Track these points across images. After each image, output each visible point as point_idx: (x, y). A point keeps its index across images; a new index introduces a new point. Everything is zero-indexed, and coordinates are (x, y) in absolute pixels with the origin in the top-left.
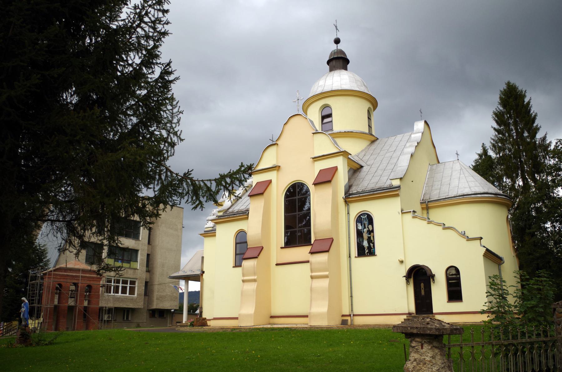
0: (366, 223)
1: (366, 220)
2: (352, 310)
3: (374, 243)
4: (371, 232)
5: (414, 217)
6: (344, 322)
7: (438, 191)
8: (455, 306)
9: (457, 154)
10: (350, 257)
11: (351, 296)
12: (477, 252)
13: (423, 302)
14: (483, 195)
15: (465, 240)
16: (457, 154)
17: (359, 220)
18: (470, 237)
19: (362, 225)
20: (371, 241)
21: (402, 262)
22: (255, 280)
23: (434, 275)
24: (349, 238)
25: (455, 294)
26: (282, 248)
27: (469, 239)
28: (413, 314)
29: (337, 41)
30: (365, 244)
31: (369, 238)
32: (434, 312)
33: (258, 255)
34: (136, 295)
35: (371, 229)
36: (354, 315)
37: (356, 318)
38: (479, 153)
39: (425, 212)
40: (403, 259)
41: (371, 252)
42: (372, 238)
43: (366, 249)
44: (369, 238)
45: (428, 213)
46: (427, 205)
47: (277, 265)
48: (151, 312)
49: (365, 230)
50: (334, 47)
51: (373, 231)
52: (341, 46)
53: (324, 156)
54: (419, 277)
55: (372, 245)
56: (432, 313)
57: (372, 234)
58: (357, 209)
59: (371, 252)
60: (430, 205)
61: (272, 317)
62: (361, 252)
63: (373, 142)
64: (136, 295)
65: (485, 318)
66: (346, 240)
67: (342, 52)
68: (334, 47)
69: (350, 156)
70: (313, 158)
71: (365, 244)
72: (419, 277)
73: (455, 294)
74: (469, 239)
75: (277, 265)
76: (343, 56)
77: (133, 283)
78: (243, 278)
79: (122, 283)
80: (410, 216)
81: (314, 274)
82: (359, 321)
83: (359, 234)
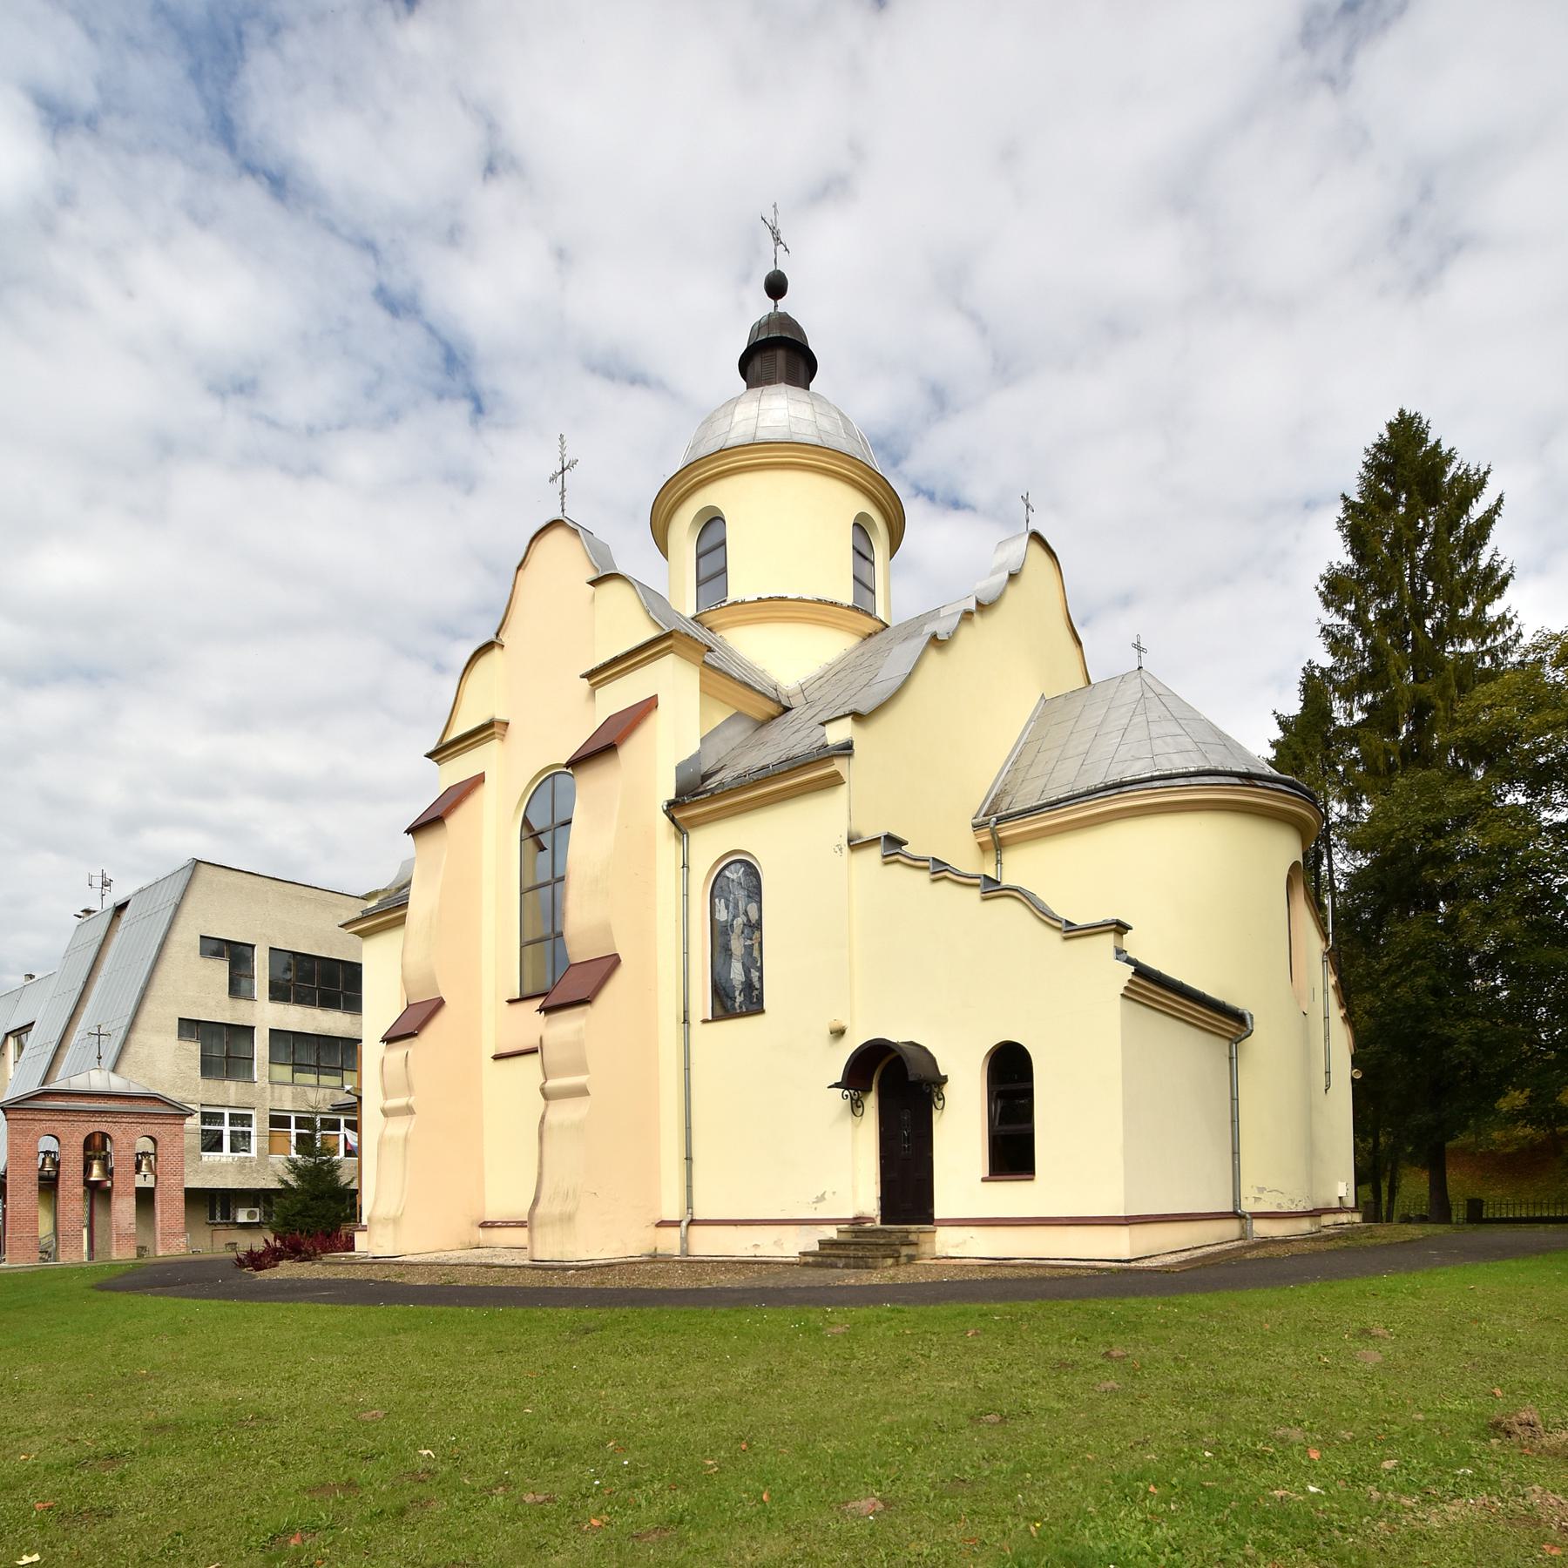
0: (741, 894)
1: (740, 883)
2: (690, 1207)
3: (761, 970)
4: (755, 926)
5: (888, 860)
7: (1043, 781)
8: (1011, 1197)
9: (1138, 647)
10: (686, 1021)
11: (689, 1158)
14: (1194, 780)
15: (1057, 936)
16: (1138, 647)
17: (718, 888)
18: (1080, 922)
19: (727, 907)
20: (754, 962)
24: (686, 953)
25: (1012, 1153)
26: (511, 1002)
27: (1071, 931)
28: (871, 1220)
29: (776, 287)
30: (737, 973)
32: (936, 1216)
34: (254, 1153)
35: (754, 916)
36: (692, 1222)
37: (696, 1231)
39: (992, 856)
41: (753, 1003)
42: (756, 954)
43: (736, 997)
45: (999, 862)
46: (993, 833)
47: (497, 1058)
49: (740, 921)
50: (762, 307)
51: (758, 926)
52: (784, 305)
55: (755, 974)
57: (757, 934)
58: (713, 842)
59: (753, 1003)
60: (1007, 830)
61: (484, 1225)
64: (254, 1153)
67: (785, 321)
68: (762, 307)
69: (709, 658)
70: (589, 675)
72: (892, 1082)
73: (1012, 1153)
74: (1071, 931)
75: (497, 1058)
77: (241, 1119)
79: (231, 1124)
80: (876, 853)
81: (551, 1084)
82: (707, 1243)
83: (720, 934)
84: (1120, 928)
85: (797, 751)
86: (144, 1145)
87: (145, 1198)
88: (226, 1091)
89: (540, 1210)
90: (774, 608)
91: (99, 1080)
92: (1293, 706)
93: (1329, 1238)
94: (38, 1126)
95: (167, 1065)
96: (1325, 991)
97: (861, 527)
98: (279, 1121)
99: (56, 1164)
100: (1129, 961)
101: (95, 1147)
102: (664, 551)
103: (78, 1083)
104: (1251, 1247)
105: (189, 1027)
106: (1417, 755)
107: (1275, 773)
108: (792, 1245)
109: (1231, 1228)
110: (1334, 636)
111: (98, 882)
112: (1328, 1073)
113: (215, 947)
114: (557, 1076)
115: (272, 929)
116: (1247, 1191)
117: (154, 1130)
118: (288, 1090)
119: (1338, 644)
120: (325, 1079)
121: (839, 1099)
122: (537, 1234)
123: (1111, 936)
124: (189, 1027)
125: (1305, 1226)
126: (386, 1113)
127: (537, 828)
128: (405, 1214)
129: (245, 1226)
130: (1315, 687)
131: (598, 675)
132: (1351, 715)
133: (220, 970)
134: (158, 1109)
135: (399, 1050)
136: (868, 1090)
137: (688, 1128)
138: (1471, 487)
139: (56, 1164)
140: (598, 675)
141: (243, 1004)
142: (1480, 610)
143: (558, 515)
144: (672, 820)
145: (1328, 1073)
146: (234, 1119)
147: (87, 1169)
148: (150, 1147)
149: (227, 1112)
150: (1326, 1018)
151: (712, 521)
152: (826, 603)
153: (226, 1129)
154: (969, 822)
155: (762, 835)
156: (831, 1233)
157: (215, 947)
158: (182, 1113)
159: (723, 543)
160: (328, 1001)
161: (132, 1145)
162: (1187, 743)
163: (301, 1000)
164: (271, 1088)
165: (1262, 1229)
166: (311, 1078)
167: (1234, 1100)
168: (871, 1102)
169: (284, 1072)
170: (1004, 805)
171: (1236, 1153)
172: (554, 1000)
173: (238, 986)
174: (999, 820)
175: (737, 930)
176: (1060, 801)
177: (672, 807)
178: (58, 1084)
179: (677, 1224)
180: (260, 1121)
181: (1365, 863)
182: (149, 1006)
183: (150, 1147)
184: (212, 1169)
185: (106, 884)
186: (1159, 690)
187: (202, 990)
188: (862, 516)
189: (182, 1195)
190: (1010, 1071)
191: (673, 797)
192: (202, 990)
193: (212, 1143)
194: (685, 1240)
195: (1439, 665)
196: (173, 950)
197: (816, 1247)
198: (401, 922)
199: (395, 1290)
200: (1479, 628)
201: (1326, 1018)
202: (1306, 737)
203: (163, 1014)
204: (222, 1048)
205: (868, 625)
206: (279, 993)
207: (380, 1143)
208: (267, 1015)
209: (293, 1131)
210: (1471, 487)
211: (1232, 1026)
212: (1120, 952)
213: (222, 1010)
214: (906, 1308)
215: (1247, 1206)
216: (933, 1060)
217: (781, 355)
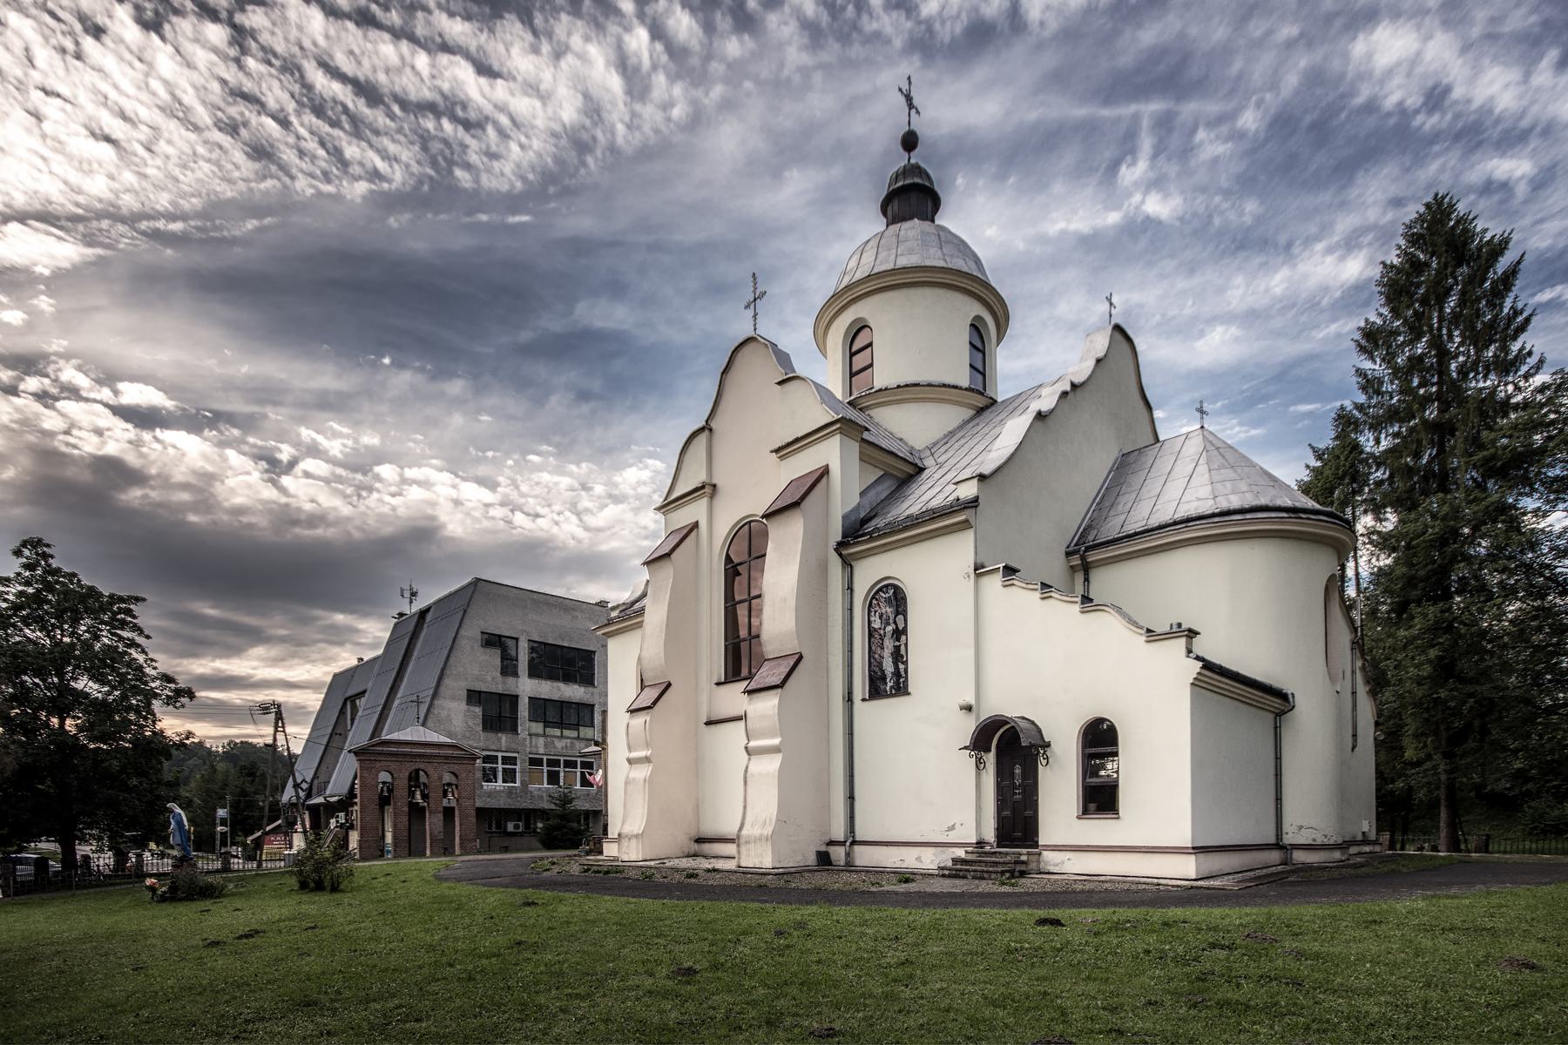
2: (852, 831)
3: (906, 663)
4: (899, 633)
6: (824, 859)
8: (1099, 830)
12: (1174, 670)
13: (1018, 820)
14: (1248, 516)
21: (969, 708)
22: (647, 760)
23: (1048, 745)
24: (851, 651)
25: (1100, 798)
30: (888, 667)
31: (897, 648)
33: (655, 703)
38: (1321, 446)
40: (973, 702)
41: (901, 689)
42: (903, 651)
43: (888, 681)
44: (897, 648)
45: (1087, 580)
46: (1083, 558)
47: (709, 723)
48: (1092, 806)
49: (889, 628)
51: (904, 632)
53: (797, 440)
54: (1008, 748)
55: (901, 666)
56: (1036, 845)
59: (901, 689)
60: (1093, 556)
62: (876, 690)
63: (980, 411)
65: (1185, 868)
66: (839, 660)
67: (916, 170)
69: (866, 435)
70: (777, 451)
71: (888, 667)
72: (1008, 748)
76: (917, 180)
78: (627, 754)
81: (753, 744)
82: (865, 857)
84: (1192, 634)
85: (934, 503)
86: (447, 778)
87: (449, 813)
88: (499, 740)
89: (744, 832)
90: (910, 392)
91: (414, 734)
92: (1326, 440)
93: (1356, 866)
94: (378, 765)
95: (456, 722)
96: (1353, 672)
97: (976, 327)
98: (535, 762)
99: (390, 791)
100: (1198, 658)
101: (414, 777)
102: (825, 355)
103: (395, 736)
104: (1293, 872)
105: (474, 697)
106: (1442, 480)
107: (1318, 506)
108: (929, 860)
109: (1275, 856)
110: (1366, 375)
111: (407, 594)
112: (1355, 736)
113: (493, 641)
114: (757, 738)
115: (526, 629)
116: (1286, 827)
117: (455, 768)
118: (541, 741)
119: (1370, 384)
120: (567, 733)
121: (967, 761)
122: (743, 849)
123: (1183, 640)
124: (474, 697)
125: (1337, 855)
126: (630, 761)
127: (736, 561)
128: (634, 827)
129: (512, 834)
130: (1346, 423)
131: (784, 450)
132: (1378, 441)
133: (494, 658)
134: (455, 756)
135: (639, 720)
136: (989, 750)
137: (851, 776)
138: (1498, 248)
139: (390, 791)
140: (784, 450)
141: (511, 680)
142: (1505, 348)
143: (752, 334)
144: (840, 555)
145: (1355, 736)
146: (505, 760)
147: (412, 794)
148: (454, 780)
149: (500, 755)
150: (1354, 693)
151: (860, 327)
152: (949, 386)
153: (500, 767)
154: (1063, 549)
155: (901, 565)
156: (960, 853)
157: (493, 641)
158: (474, 758)
159: (870, 345)
160: (568, 678)
161: (440, 778)
162: (1243, 486)
163: (552, 676)
164: (531, 738)
165: (1299, 856)
166: (557, 732)
167: (1278, 759)
168: (990, 758)
169: (538, 727)
170: (1091, 538)
171: (1279, 799)
172: (753, 685)
173: (509, 668)
174: (1088, 549)
175: (889, 635)
176: (1136, 534)
177: (840, 546)
178: (385, 736)
179: (843, 843)
180: (523, 761)
181: (1389, 561)
182: (447, 681)
183: (454, 780)
184: (490, 794)
185: (414, 594)
186: (1219, 444)
187: (480, 669)
188: (978, 318)
189: (473, 813)
190: (1100, 739)
191: (839, 538)
192: (480, 669)
193: (490, 776)
194: (848, 855)
195: (1462, 401)
196: (463, 643)
197: (950, 864)
198: (640, 625)
199: (615, 879)
200: (1498, 121)
201: (1354, 693)
202: (1339, 476)
203: (456, 686)
204: (497, 712)
205: (980, 402)
206: (534, 673)
207: (627, 783)
208: (527, 687)
209: (545, 769)
210: (1498, 248)
211: (1277, 702)
212: (1189, 651)
213: (492, 681)
214: (567, 895)
215: (1288, 839)
216: (1040, 731)
217: (914, 197)
